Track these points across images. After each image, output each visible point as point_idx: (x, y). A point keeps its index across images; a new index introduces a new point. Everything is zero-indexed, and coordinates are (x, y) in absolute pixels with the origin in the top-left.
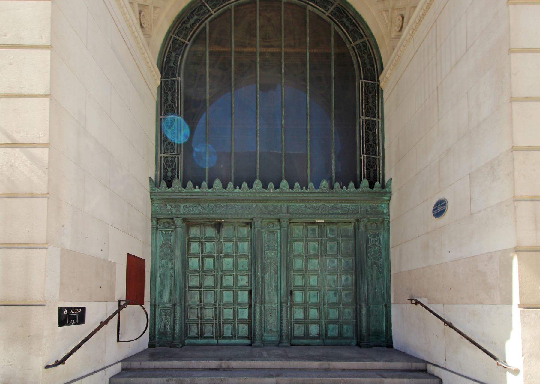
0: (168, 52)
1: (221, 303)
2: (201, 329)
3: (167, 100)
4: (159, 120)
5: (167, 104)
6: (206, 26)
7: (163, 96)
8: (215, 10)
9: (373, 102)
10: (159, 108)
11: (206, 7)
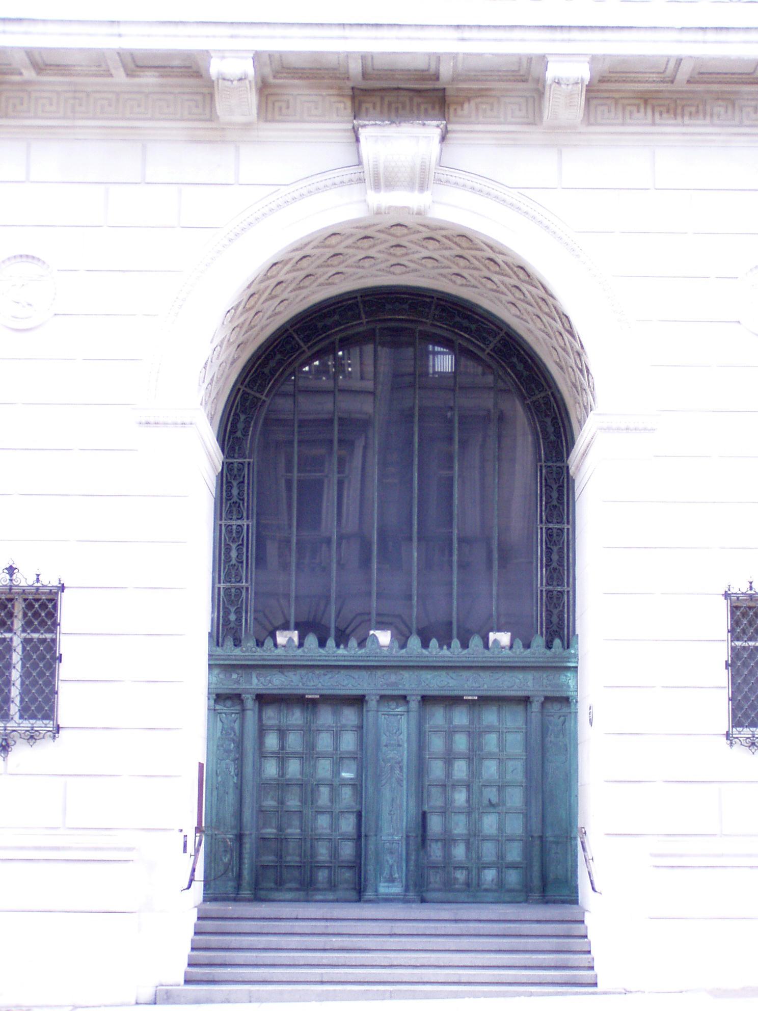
5: (232, 501)
9: (558, 498)
10: (219, 505)
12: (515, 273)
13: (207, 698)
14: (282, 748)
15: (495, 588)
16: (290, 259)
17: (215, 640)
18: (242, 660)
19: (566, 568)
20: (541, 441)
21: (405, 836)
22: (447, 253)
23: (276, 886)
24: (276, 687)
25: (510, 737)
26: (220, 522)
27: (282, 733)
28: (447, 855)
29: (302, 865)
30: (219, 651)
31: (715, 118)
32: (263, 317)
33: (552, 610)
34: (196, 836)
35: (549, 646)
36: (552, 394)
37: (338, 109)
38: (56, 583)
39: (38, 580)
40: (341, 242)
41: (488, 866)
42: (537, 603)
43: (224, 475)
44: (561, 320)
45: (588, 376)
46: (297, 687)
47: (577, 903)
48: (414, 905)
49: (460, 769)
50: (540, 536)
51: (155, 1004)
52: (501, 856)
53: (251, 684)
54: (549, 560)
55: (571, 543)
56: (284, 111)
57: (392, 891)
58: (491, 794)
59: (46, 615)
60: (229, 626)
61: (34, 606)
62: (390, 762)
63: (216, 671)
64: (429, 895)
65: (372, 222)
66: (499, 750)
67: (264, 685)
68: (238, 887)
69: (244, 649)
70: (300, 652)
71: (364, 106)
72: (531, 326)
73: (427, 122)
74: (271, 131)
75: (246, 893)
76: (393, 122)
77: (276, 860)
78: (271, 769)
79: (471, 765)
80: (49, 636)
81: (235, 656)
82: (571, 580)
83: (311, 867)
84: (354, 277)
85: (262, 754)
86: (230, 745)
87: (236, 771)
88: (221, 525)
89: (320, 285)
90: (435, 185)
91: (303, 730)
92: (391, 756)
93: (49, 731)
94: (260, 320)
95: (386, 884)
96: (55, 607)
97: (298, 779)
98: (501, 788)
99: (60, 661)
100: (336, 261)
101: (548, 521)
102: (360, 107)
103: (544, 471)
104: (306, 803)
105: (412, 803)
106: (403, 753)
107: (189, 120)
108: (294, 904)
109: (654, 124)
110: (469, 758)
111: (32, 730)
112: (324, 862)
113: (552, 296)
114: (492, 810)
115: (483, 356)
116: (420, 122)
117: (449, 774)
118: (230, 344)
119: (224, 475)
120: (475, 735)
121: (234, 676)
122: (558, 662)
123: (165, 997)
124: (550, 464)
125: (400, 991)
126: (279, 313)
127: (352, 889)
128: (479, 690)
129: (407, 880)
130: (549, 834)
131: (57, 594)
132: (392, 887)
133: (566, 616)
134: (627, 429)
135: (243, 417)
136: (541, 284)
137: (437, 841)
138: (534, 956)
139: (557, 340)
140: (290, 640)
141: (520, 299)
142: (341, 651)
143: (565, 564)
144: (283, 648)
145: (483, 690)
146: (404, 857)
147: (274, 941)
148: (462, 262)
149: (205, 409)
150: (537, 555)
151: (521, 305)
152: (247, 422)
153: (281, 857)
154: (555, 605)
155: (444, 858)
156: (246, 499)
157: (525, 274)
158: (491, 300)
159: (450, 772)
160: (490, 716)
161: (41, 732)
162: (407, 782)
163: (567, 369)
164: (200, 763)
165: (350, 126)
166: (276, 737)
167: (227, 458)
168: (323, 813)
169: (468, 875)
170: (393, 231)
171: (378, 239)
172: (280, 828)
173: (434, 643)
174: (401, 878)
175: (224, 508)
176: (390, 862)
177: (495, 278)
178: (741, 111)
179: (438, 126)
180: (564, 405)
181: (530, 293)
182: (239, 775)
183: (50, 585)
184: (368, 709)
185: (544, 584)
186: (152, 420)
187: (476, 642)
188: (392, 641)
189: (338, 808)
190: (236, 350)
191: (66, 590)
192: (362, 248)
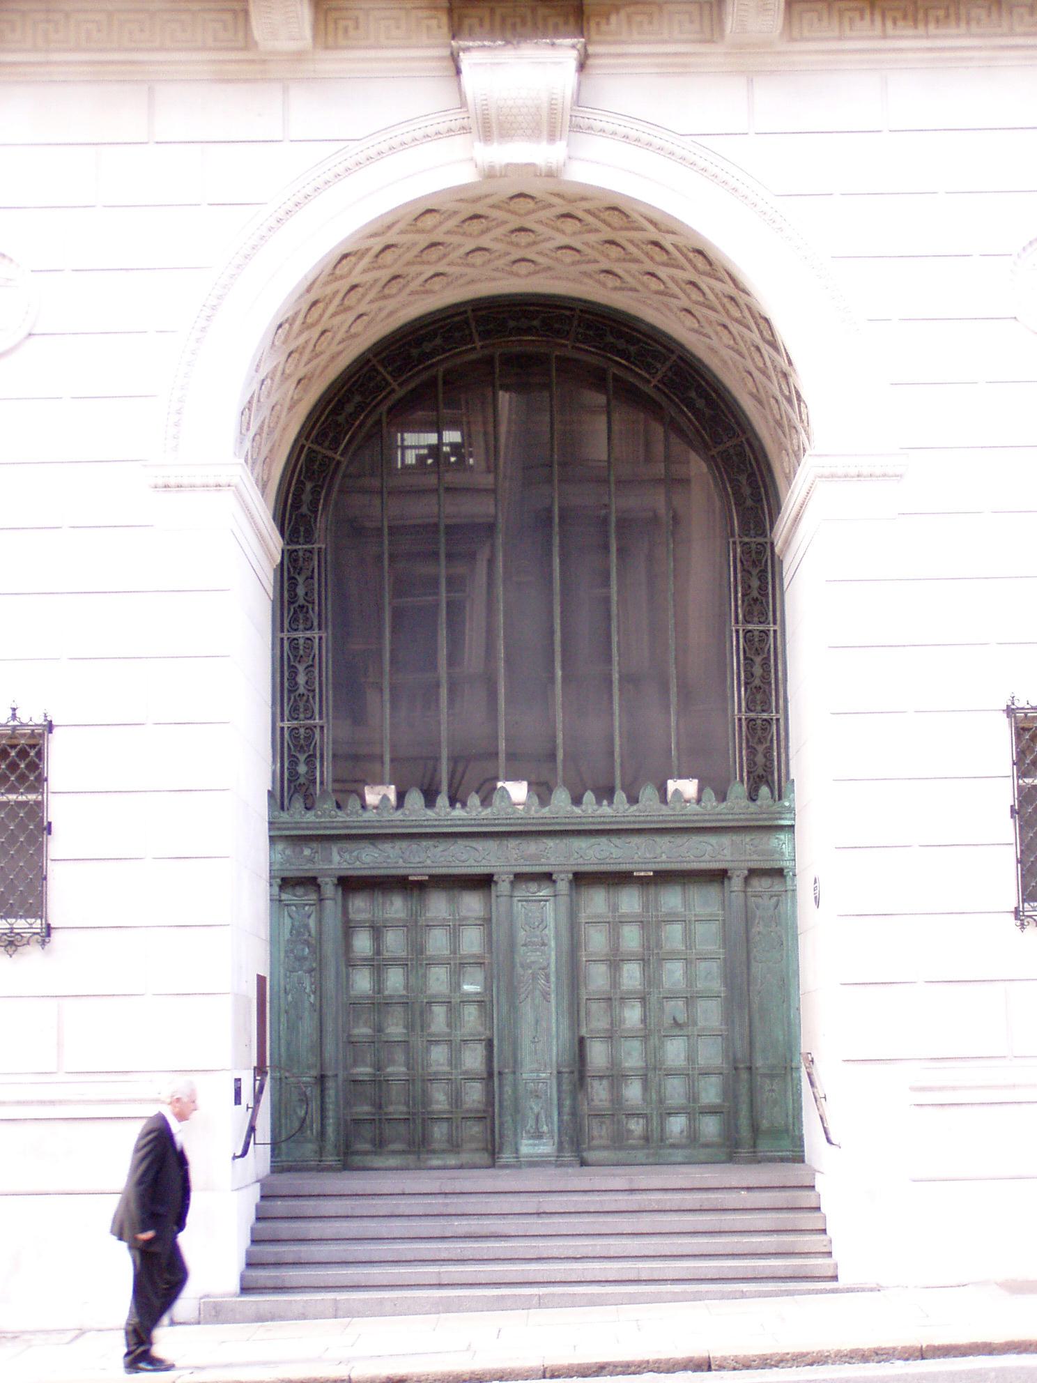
1: (422, 1031)
5: (296, 605)
8: (400, 380)
12: (690, 261)
13: (268, 885)
14: (378, 952)
15: (673, 718)
16: (368, 250)
17: (278, 801)
18: (317, 829)
19: (773, 686)
20: (734, 507)
21: (555, 1072)
22: (592, 238)
23: (374, 1149)
24: (366, 866)
25: (700, 929)
26: (280, 635)
27: (377, 931)
28: (617, 1098)
29: (410, 1117)
30: (285, 817)
31: (973, 24)
32: (333, 339)
33: (756, 746)
34: (255, 1080)
35: (753, 797)
36: (748, 440)
37: (429, 28)
38: (40, 720)
39: (14, 717)
40: (441, 223)
41: (676, 1113)
42: (735, 738)
43: (285, 567)
44: (758, 325)
45: (799, 405)
46: (396, 865)
47: (803, 1161)
48: (570, 1170)
49: (632, 975)
50: (736, 642)
51: (199, 1323)
52: (693, 1097)
53: (331, 862)
54: (750, 675)
55: (779, 650)
56: (352, 32)
57: (539, 1151)
58: (676, 1008)
59: (27, 766)
60: (298, 782)
61: (9, 753)
62: (531, 968)
63: (280, 846)
64: (591, 1156)
65: (484, 190)
66: (686, 946)
67: (349, 864)
68: (321, 1151)
69: (319, 813)
70: (398, 815)
71: (467, 22)
72: (715, 343)
73: (558, 41)
74: (330, 62)
75: (330, 1160)
76: (508, 42)
77: (373, 1110)
78: (362, 982)
79: (646, 969)
80: (32, 797)
81: (307, 823)
82: (781, 702)
83: (423, 1119)
84: (461, 281)
85: (350, 962)
86: (303, 950)
87: (313, 986)
88: (282, 639)
89: (412, 293)
90: (572, 134)
91: (407, 926)
92: (533, 959)
93: (35, 934)
94: (329, 344)
95: (531, 1142)
96: (40, 755)
97: (401, 996)
98: (690, 1000)
99: (50, 833)
100: (434, 254)
101: (747, 621)
102: (460, 26)
103: (739, 550)
104: (413, 1030)
105: (565, 1023)
106: (550, 954)
107: (210, 49)
108: (654, 1167)
109: (885, 37)
110: (643, 960)
111: (11, 932)
112: (440, 1112)
113: (744, 291)
114: (676, 1031)
115: (648, 389)
116: (548, 41)
117: (615, 983)
118: (287, 379)
119: (285, 567)
120: (650, 925)
121: (307, 852)
122: (765, 820)
123: (213, 1313)
124: (746, 539)
125: (553, 1295)
126: (355, 336)
127: (483, 1149)
128: (655, 863)
129: (560, 1136)
130: (759, 1063)
131: (41, 735)
132: (538, 1145)
133: (775, 754)
134: (858, 476)
135: (309, 486)
136: (728, 273)
137: (601, 1077)
138: (745, 1239)
139: (753, 359)
140: (385, 798)
141: (697, 303)
142: (458, 812)
143: (773, 681)
144: (375, 811)
145: (662, 862)
146: (555, 1102)
147: (372, 1228)
148: (614, 252)
149: (252, 470)
150: (733, 669)
151: (700, 311)
152: (315, 492)
153: (380, 1107)
154: (759, 739)
155: (612, 1101)
156: (316, 601)
157: (705, 261)
158: (657, 309)
159: (617, 981)
160: (672, 899)
161: (23, 935)
162: (557, 995)
163: (768, 401)
164: (258, 976)
165: (446, 52)
166: (368, 936)
167: (288, 544)
168: (437, 1042)
169: (647, 1126)
170: (514, 205)
171: (494, 220)
172: (378, 1067)
173: (589, 797)
174: (551, 1131)
175: (286, 615)
176: (536, 1110)
177: (663, 272)
178: (1011, 13)
179: (573, 47)
180: (765, 456)
181: (712, 290)
182: (318, 993)
183: (31, 723)
184: (499, 893)
185: (743, 710)
186: (172, 482)
187: (648, 794)
188: (529, 797)
189: (458, 1035)
190: (296, 388)
191: (55, 731)
192: (471, 235)
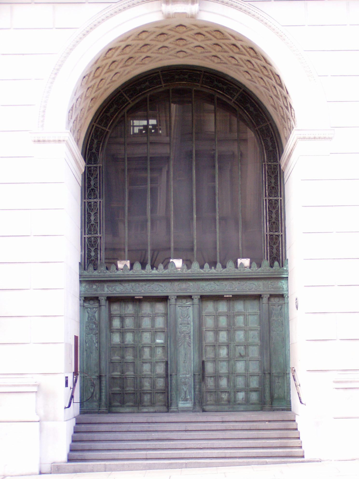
0: (91, 140)
2: (123, 398)
3: (90, 185)
4: (83, 203)
5: (91, 189)
6: (124, 114)
7: (86, 181)
11: (125, 96)
